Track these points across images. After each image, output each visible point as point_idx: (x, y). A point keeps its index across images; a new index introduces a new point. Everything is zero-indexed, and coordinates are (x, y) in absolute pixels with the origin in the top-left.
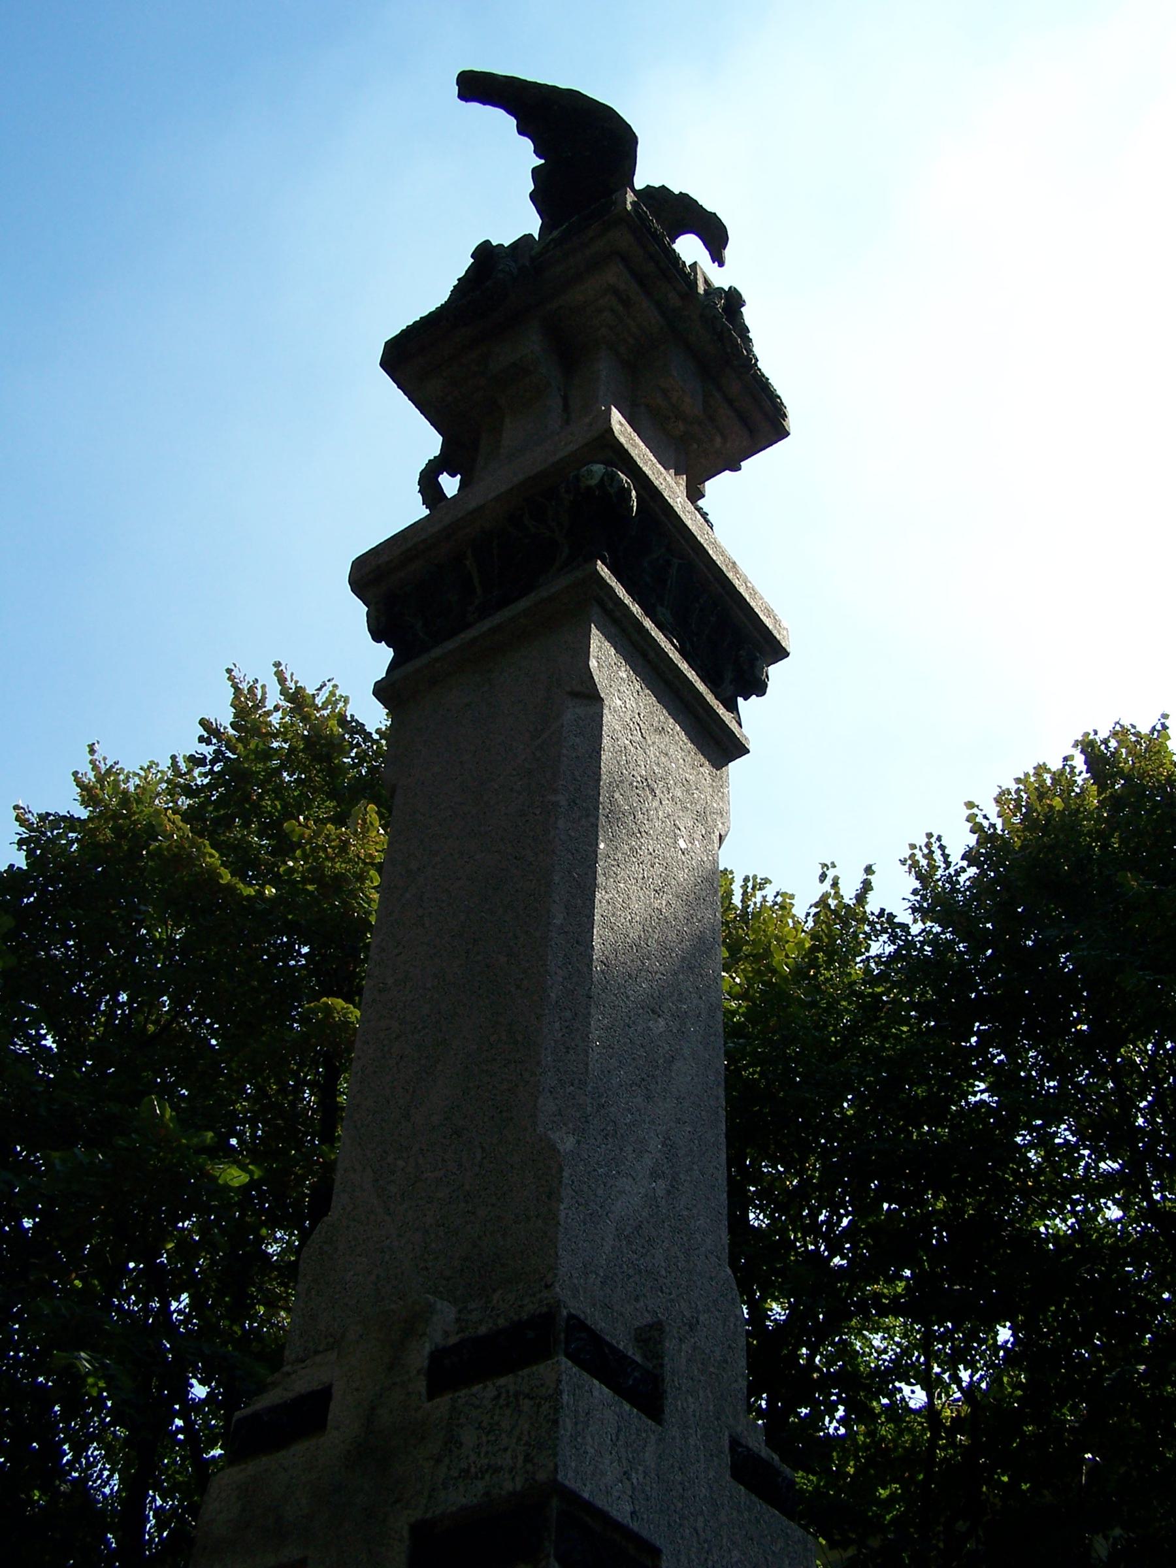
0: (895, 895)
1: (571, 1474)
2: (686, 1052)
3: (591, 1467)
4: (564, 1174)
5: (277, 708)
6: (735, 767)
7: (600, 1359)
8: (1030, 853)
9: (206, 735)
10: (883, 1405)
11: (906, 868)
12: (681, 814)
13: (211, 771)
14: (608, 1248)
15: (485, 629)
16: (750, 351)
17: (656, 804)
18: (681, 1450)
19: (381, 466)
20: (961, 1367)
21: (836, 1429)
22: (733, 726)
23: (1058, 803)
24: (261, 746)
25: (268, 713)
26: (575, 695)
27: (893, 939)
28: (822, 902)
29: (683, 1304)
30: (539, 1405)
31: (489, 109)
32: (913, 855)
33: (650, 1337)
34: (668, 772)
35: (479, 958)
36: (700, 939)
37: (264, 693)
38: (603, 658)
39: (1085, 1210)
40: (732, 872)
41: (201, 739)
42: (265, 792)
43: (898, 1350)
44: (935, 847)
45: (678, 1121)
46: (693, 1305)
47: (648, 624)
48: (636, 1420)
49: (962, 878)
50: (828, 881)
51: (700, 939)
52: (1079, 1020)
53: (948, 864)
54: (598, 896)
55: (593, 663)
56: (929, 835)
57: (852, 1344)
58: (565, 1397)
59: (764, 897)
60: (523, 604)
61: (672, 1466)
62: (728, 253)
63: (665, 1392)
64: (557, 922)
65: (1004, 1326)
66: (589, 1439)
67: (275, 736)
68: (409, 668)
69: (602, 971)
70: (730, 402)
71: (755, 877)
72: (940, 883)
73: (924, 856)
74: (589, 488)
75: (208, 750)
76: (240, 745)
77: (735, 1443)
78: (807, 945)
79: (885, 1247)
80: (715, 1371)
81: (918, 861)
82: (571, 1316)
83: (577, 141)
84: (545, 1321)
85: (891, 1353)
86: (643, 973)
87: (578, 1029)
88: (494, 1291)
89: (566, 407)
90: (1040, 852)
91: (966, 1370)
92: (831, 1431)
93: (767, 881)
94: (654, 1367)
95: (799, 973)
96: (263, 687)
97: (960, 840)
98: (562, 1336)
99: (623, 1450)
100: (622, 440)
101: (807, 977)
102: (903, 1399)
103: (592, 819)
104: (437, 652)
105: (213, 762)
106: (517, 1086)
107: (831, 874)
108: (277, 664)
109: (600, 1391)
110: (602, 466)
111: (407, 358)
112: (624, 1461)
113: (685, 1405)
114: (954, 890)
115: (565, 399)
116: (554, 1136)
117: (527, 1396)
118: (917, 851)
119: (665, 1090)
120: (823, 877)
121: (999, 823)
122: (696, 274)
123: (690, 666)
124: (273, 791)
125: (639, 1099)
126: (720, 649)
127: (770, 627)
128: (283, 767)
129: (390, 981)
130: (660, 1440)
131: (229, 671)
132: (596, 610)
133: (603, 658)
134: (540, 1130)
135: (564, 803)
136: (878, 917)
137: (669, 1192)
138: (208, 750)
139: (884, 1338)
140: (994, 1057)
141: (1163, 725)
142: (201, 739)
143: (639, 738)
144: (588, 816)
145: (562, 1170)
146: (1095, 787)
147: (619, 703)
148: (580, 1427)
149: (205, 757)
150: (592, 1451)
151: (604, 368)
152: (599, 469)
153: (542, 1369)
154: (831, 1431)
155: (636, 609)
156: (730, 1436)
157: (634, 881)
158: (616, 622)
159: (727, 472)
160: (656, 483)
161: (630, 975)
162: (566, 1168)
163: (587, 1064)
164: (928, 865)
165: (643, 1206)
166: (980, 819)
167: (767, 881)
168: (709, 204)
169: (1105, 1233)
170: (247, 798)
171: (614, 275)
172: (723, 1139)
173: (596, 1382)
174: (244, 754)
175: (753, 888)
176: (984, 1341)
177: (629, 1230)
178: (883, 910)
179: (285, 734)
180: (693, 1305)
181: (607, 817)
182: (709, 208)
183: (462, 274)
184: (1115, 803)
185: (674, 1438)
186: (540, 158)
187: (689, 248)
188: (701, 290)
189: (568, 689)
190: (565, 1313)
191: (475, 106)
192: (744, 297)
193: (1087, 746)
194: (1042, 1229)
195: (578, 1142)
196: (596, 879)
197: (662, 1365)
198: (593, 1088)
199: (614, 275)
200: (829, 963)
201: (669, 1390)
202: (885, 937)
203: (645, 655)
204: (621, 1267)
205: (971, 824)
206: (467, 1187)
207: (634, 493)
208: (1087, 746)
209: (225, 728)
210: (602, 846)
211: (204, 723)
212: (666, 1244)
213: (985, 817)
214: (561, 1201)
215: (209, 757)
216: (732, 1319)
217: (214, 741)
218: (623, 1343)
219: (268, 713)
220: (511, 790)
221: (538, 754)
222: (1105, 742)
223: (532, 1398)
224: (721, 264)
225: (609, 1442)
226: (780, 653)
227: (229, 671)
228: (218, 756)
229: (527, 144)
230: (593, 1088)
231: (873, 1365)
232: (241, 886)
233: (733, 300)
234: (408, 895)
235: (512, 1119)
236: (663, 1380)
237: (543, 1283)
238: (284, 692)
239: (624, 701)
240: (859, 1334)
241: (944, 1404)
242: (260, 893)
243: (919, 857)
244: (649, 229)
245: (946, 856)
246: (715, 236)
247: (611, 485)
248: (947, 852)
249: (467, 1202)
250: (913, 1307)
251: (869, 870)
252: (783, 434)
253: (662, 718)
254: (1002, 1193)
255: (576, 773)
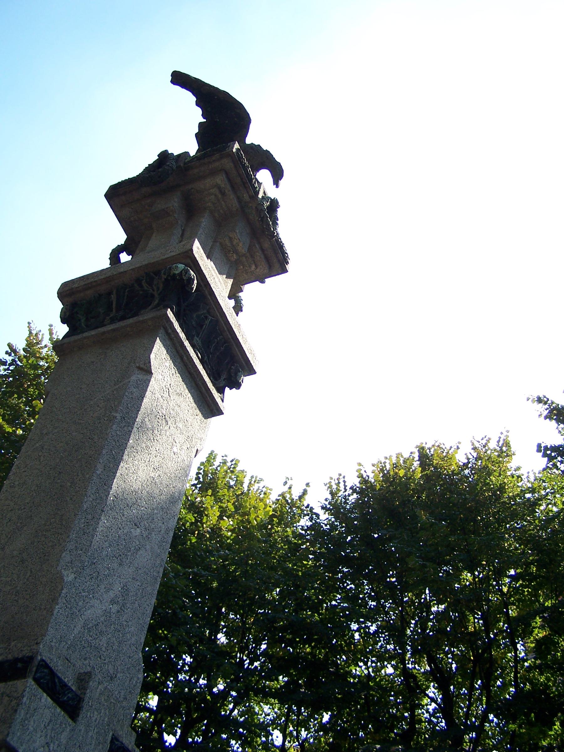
0: (317, 499)
1: (15, 739)
2: (148, 547)
3: (28, 737)
4: (63, 591)
5: (46, 346)
6: (215, 420)
7: (52, 685)
8: (382, 493)
9: (10, 351)
10: (262, 741)
11: (326, 487)
12: (179, 435)
13: (8, 369)
14: (76, 631)
15: (110, 328)
16: (275, 229)
17: (167, 428)
18: (83, 737)
19: (94, 242)
20: (303, 729)
21: (238, 748)
22: (218, 400)
23: (402, 473)
24: (35, 362)
25: (42, 348)
26: (139, 368)
27: (311, 519)
28: (283, 495)
29: (110, 666)
30: (11, 701)
31: (184, 90)
32: (330, 482)
33: (84, 679)
34: (178, 414)
35: (59, 481)
36: (171, 495)
37: (42, 338)
38: (159, 355)
39: (376, 666)
40: (246, 472)
41: (7, 353)
42: (32, 385)
43: (275, 715)
44: (341, 481)
45: (133, 579)
46: (116, 668)
47: (187, 344)
48: (62, 718)
49: (350, 498)
50: (288, 486)
51: (171, 495)
52: (392, 576)
53: (346, 490)
54: (122, 464)
55: (152, 356)
56: (340, 475)
57: (254, 708)
58: (25, 699)
59: (259, 487)
60: (131, 321)
61: (75, 744)
62: (281, 182)
63: (83, 707)
64: (98, 472)
65: (327, 714)
66: (32, 723)
67: (42, 359)
68: (73, 338)
69: (113, 500)
70: (263, 250)
71: (256, 477)
72: (340, 498)
73: (335, 484)
74: (174, 274)
75: (9, 359)
76: (25, 360)
77: (114, 739)
78: (271, 513)
79: (279, 665)
80: (114, 702)
81: (332, 486)
82: (42, 660)
83: (222, 115)
84: (28, 661)
85: (271, 716)
86: (135, 506)
87: (92, 525)
88: (14, 641)
89: (182, 235)
90: (387, 493)
91: (305, 731)
92: (235, 749)
93: (261, 480)
94: (81, 694)
95: (262, 526)
96: (43, 334)
97: (353, 481)
98: (34, 669)
99: (49, 731)
100: (196, 256)
101: (266, 528)
102: (272, 740)
103: (130, 428)
104: (86, 334)
105: (10, 365)
106: (56, 545)
107: (289, 483)
108: (51, 326)
109: (46, 699)
110: (184, 266)
111: (118, 196)
112: (48, 737)
113: (92, 716)
114: (346, 503)
115: (183, 231)
116: (65, 573)
117: (8, 696)
118: (333, 481)
119: (131, 563)
120: (286, 483)
121: (371, 475)
122: (260, 188)
123: (204, 368)
124: (35, 385)
125: (116, 565)
126: (221, 363)
127: (250, 359)
128: (42, 374)
129: (17, 483)
130: (73, 730)
131: (29, 323)
132: (162, 331)
133: (159, 355)
134: (59, 568)
135: (119, 418)
136: (306, 508)
137: (118, 612)
138: (9, 359)
139: (270, 708)
140: (348, 585)
141: (458, 446)
142: (7, 353)
143: (166, 395)
144: (128, 426)
145: (62, 589)
146: (420, 469)
147: (161, 377)
148: (28, 716)
149: (7, 362)
150: (32, 729)
151: (205, 221)
152: (181, 266)
153: (19, 684)
154: (235, 749)
155: (182, 335)
156: (113, 735)
157: (143, 462)
158: (171, 339)
159: (258, 282)
160: (209, 279)
161: (128, 505)
162: (65, 589)
163: (92, 542)
164: (336, 488)
165: (102, 617)
166: (362, 472)
167: (261, 480)
168: (278, 158)
169: (383, 679)
170: (22, 386)
171: (220, 180)
172: (156, 592)
173: (45, 695)
174: (25, 364)
175: (255, 482)
176: (317, 719)
177: (91, 625)
178: (308, 505)
179: (47, 359)
180: (116, 668)
181: (138, 429)
182: (278, 159)
183: (151, 162)
184: (427, 478)
185: (80, 730)
186: (204, 118)
187: (264, 176)
188: (260, 196)
189: (138, 365)
190: (39, 658)
191: (178, 88)
192: (280, 204)
193: (421, 449)
194: (354, 671)
195: (76, 578)
196: (123, 456)
197: (85, 694)
198: (91, 554)
199: (220, 180)
200: (279, 524)
201: (85, 706)
202: (307, 517)
203: (182, 358)
204: (81, 642)
205: (358, 473)
206: (18, 588)
207: (195, 282)
208: (421, 449)
209: (19, 350)
210: (131, 442)
211: (10, 345)
212: (109, 636)
213: (365, 471)
214: (57, 604)
215: (9, 362)
216: (135, 679)
217: (13, 355)
218: (69, 679)
219: (42, 348)
220: (98, 406)
221: (115, 392)
222: (429, 449)
223: (9, 697)
224: (277, 187)
225: (42, 726)
226: (251, 371)
227: (29, 323)
228: (13, 362)
229: (199, 111)
230: (91, 554)
231: (261, 720)
232: (6, 426)
233: (274, 205)
234: (37, 445)
235: (48, 560)
236: (83, 701)
237: (36, 641)
238: (51, 339)
239: (164, 377)
240: (258, 704)
241: (291, 746)
242: (14, 432)
243: (333, 484)
244: (241, 163)
245: (345, 486)
246: (277, 173)
247: (185, 275)
248: (346, 484)
249: (16, 595)
250: (283, 696)
251: (308, 485)
252: (285, 271)
253: (182, 390)
254: (336, 650)
255: (129, 405)
